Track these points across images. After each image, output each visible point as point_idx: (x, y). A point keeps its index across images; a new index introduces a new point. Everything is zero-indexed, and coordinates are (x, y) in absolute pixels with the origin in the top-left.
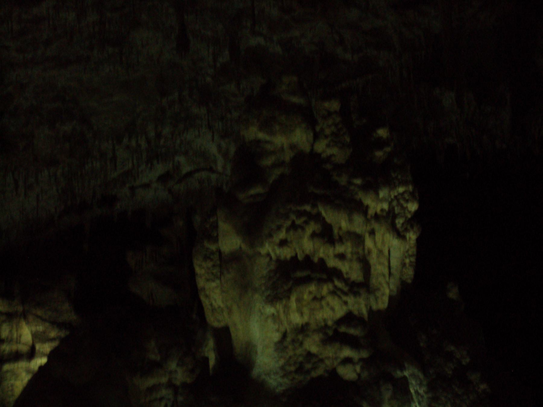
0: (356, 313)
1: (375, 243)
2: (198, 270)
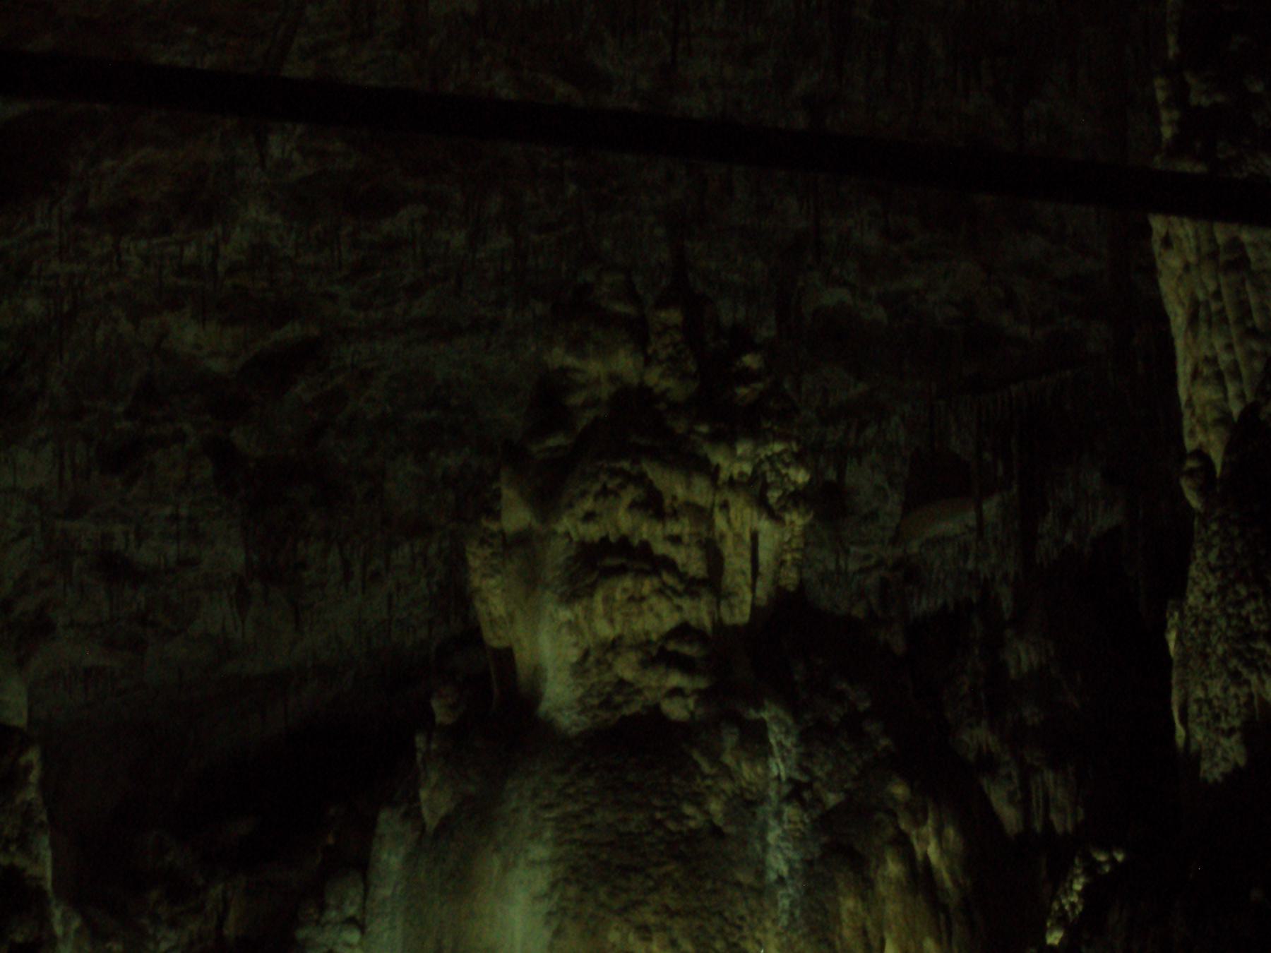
0: (693, 623)
1: (729, 521)
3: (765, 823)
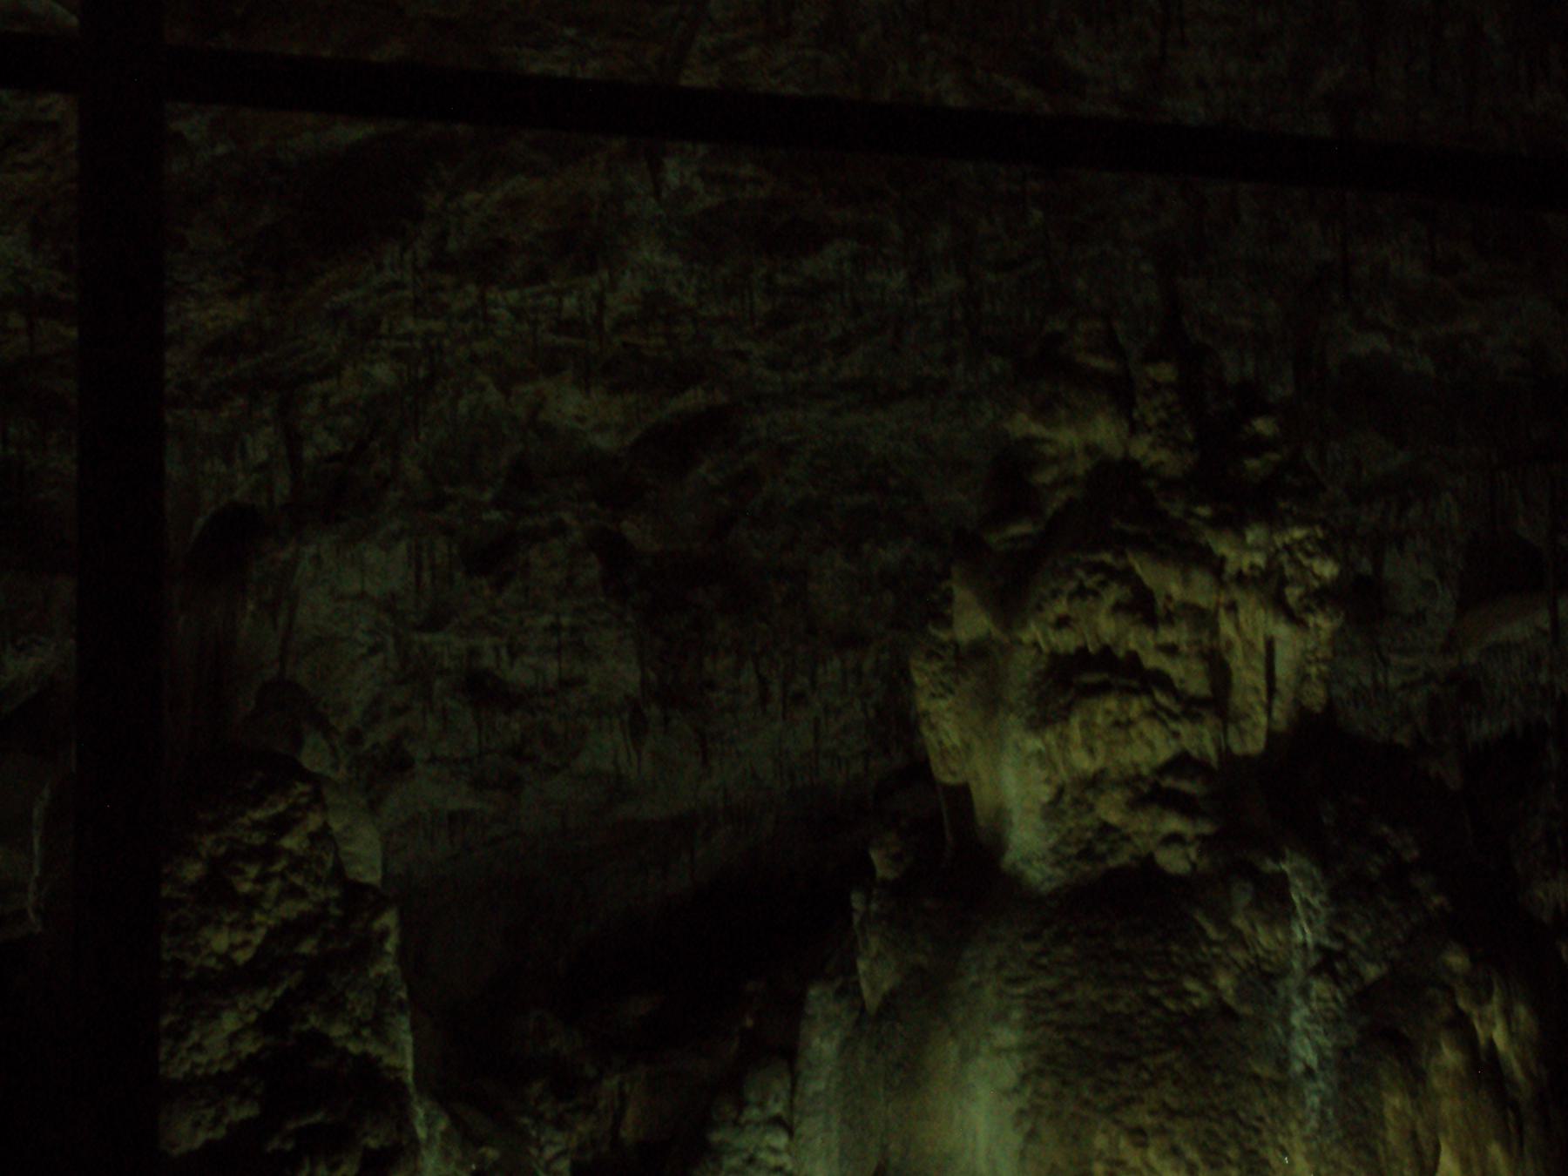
0: (1195, 753)
1: (1237, 627)
2: (918, 679)
3: (1288, 1001)
